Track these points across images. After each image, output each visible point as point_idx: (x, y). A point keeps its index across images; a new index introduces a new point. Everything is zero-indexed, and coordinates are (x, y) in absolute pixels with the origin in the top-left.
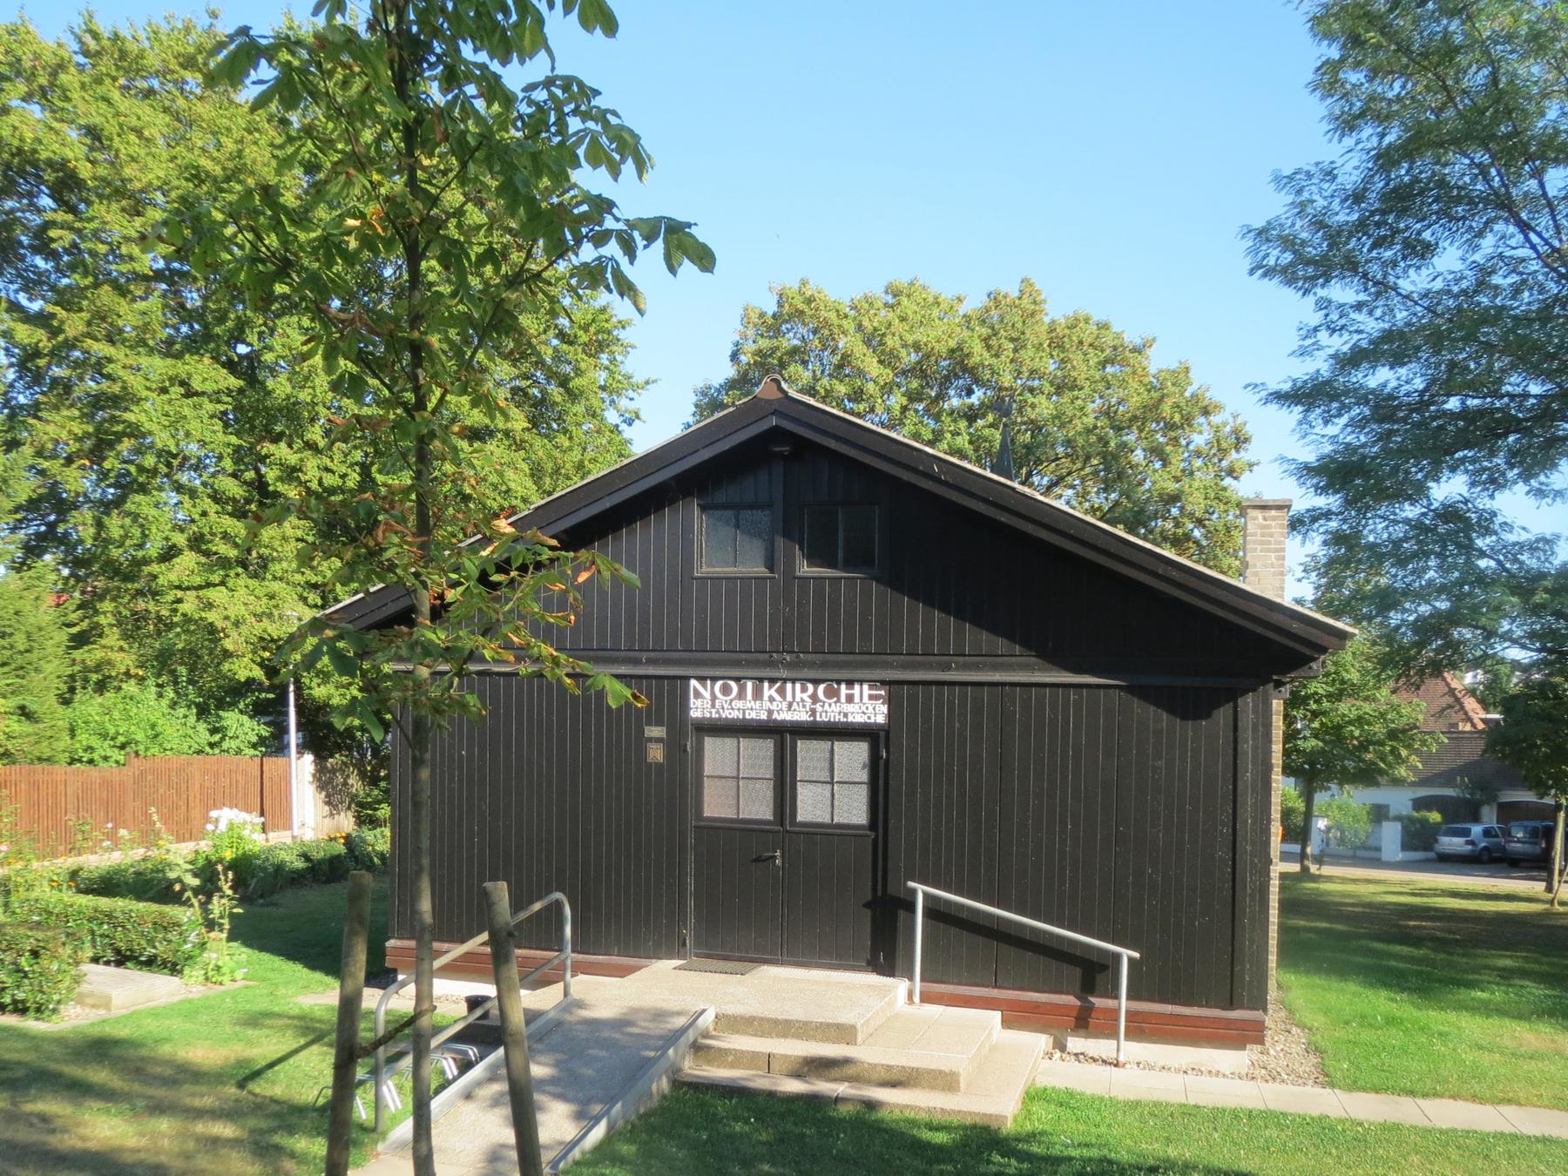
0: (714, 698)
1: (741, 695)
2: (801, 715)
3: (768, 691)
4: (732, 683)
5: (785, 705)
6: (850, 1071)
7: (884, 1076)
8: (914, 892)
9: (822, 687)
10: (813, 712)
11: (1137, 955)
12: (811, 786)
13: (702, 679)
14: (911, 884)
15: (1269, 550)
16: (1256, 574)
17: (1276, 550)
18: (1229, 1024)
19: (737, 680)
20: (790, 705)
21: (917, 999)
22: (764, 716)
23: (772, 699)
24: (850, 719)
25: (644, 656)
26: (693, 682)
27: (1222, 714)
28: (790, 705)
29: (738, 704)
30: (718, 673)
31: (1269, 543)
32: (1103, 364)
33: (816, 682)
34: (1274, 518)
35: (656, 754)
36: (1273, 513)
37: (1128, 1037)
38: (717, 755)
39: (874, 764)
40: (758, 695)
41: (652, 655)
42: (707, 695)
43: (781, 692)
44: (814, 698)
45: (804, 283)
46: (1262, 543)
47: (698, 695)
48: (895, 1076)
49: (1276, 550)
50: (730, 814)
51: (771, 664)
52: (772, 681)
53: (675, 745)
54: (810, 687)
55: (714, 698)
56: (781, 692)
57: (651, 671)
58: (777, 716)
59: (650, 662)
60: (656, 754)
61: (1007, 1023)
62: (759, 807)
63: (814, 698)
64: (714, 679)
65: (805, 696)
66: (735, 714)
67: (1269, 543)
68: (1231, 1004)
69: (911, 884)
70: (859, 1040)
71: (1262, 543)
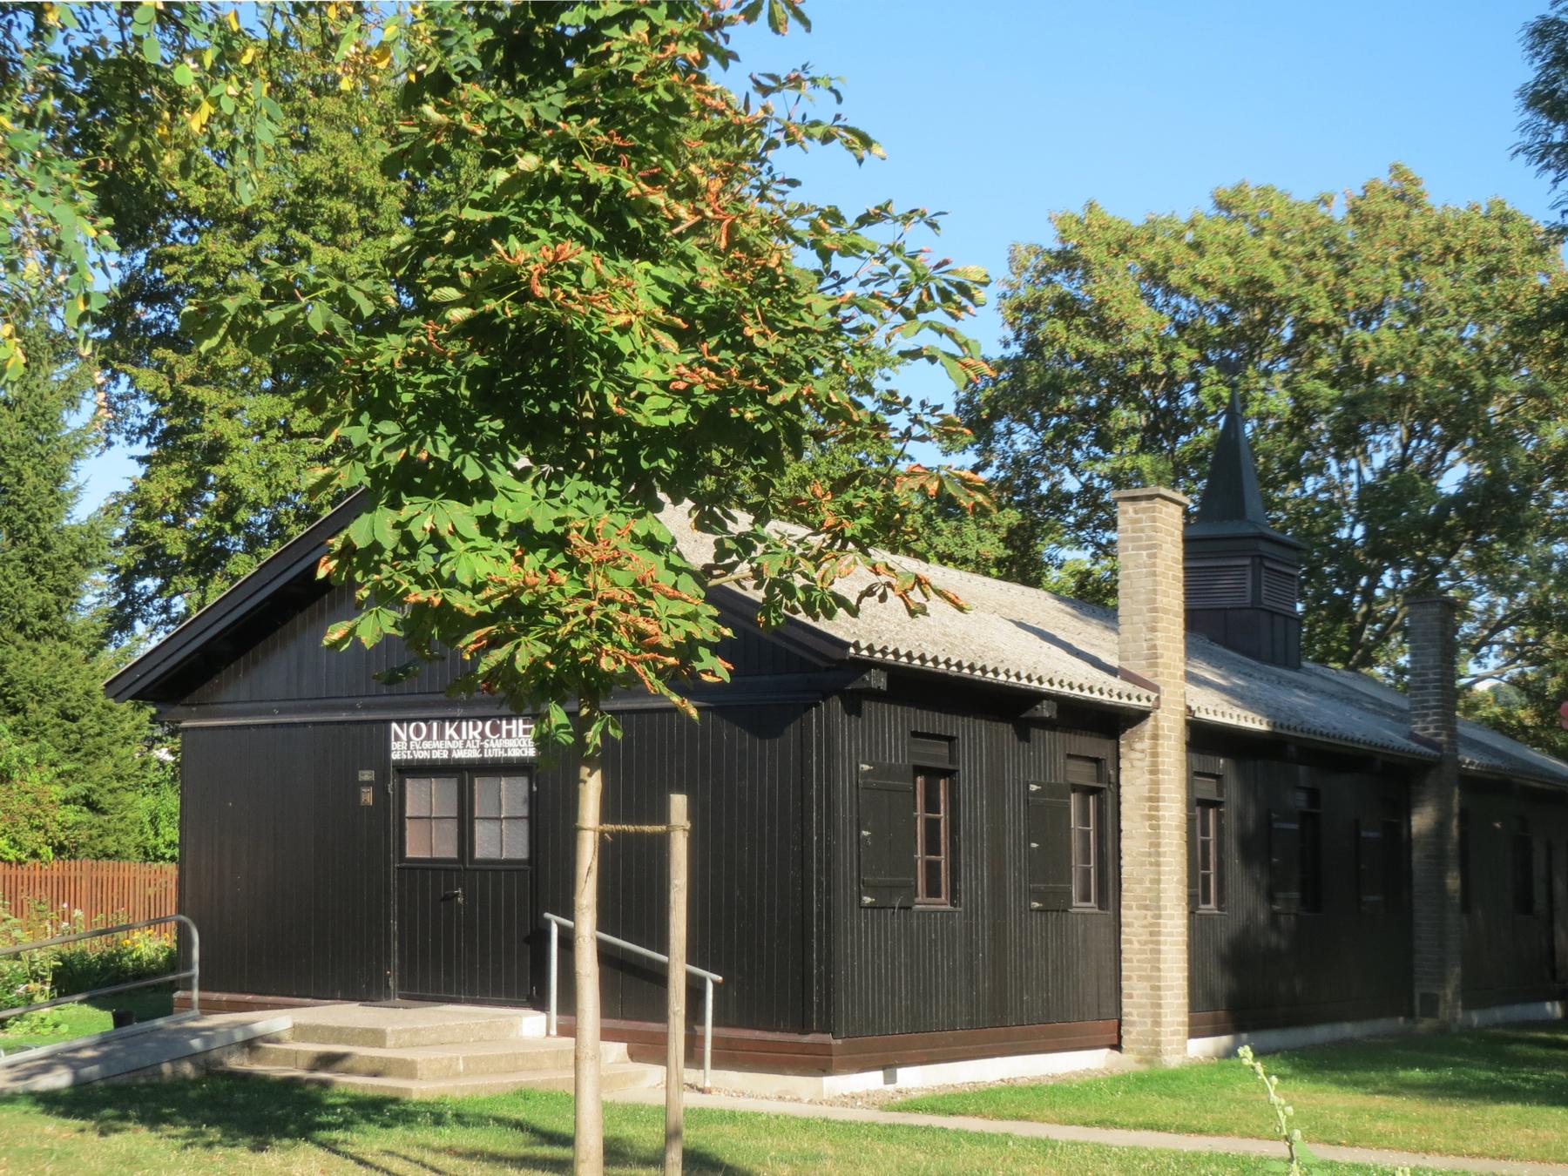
0: (409, 739)
1: (429, 737)
2: (472, 753)
3: (449, 730)
4: (423, 725)
5: (460, 744)
6: (347, 1064)
7: (371, 1067)
8: (548, 922)
9: (488, 724)
10: (482, 748)
11: (720, 978)
12: (486, 824)
13: (400, 722)
14: (547, 915)
15: (1140, 548)
16: (1128, 577)
17: (1149, 547)
18: (804, 1049)
19: (426, 720)
20: (465, 743)
21: (554, 1032)
22: (445, 756)
23: (451, 739)
24: (510, 754)
25: (359, 703)
26: (394, 726)
27: (792, 730)
28: (465, 743)
29: (427, 745)
30: (411, 715)
31: (1140, 539)
32: (1487, 276)
33: (484, 719)
34: (1145, 510)
35: (367, 797)
36: (1144, 504)
37: (716, 1064)
38: (419, 797)
39: (533, 801)
40: (441, 736)
41: (367, 700)
42: (403, 736)
43: (458, 730)
44: (482, 734)
45: (1091, 206)
46: (1133, 540)
47: (397, 738)
48: (377, 1066)
49: (1149, 547)
50: (424, 854)
51: (452, 704)
52: (452, 720)
53: (379, 787)
54: (480, 724)
55: (409, 739)
56: (458, 730)
57: (364, 716)
58: (457, 755)
59: (366, 708)
60: (367, 797)
61: (634, 1056)
62: (447, 849)
63: (482, 734)
64: (409, 721)
65: (476, 734)
66: (424, 755)
67: (1140, 539)
68: (805, 1028)
69: (547, 915)
70: (388, 1043)
71: (1133, 540)
